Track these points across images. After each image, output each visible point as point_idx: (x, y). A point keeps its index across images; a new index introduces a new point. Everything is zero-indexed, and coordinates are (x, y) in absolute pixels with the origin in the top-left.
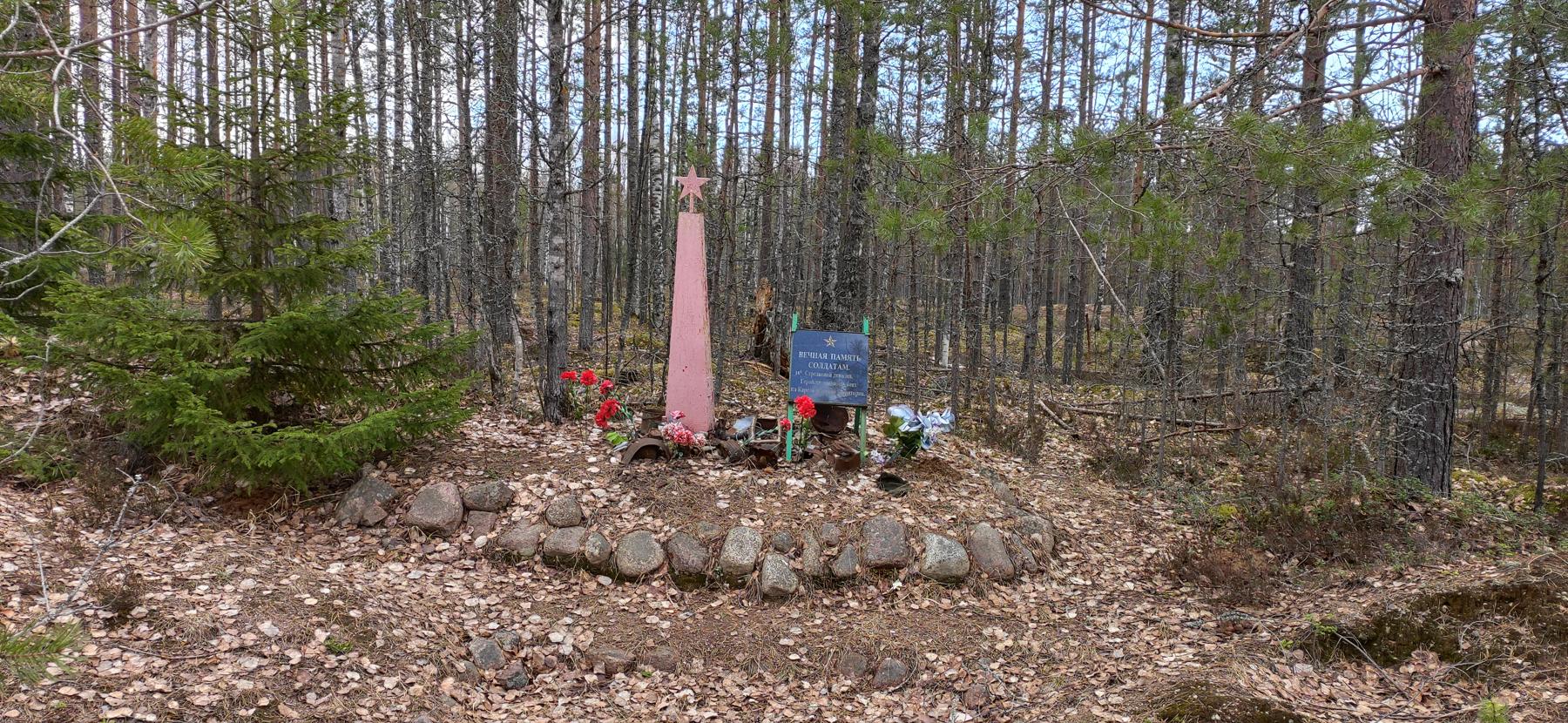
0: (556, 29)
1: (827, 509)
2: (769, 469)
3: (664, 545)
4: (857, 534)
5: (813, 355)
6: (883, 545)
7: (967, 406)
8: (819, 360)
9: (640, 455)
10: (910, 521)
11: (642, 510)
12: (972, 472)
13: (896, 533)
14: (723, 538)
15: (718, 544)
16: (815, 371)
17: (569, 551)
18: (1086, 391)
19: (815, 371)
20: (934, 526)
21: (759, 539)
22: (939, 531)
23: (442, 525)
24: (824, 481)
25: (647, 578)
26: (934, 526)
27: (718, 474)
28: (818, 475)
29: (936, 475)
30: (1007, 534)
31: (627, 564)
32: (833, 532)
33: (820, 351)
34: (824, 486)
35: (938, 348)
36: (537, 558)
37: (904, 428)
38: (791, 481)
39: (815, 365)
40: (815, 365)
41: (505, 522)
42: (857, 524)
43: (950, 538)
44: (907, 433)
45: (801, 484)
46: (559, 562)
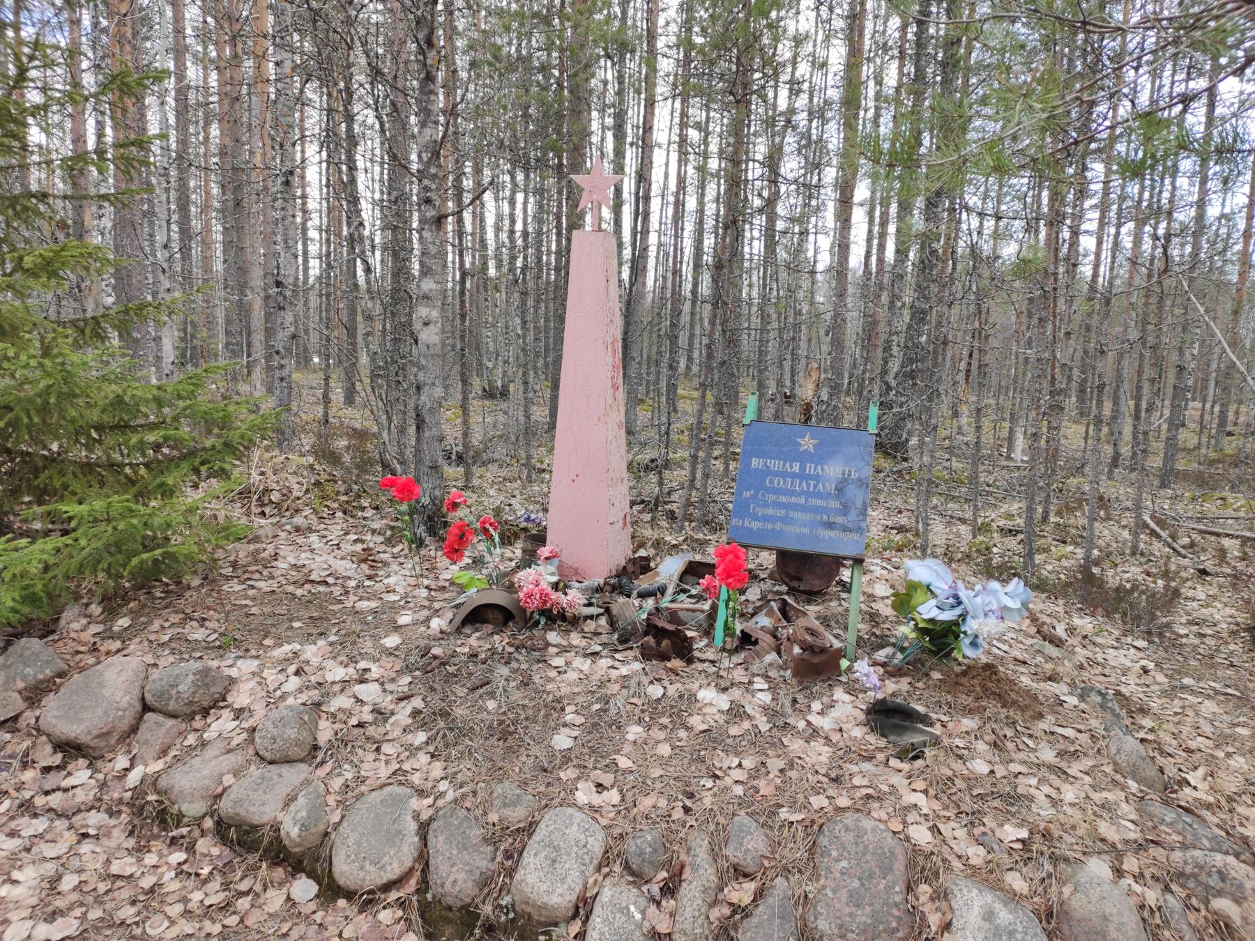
0: (770, 232)
1: (755, 774)
2: (676, 663)
3: (424, 829)
4: (802, 854)
5: (775, 465)
6: (856, 900)
7: (1045, 519)
8: (784, 475)
9: (477, 616)
10: (921, 835)
11: (421, 737)
12: (1061, 689)
13: (886, 870)
14: (530, 828)
15: (511, 843)
16: (778, 492)
17: (256, 820)
18: (1193, 499)
19: (778, 492)
20: (977, 855)
21: (596, 845)
22: (988, 877)
23: (84, 739)
24: (766, 698)
25: (368, 901)
26: (977, 855)
27: (586, 665)
28: (760, 683)
29: (993, 707)
30: (1152, 896)
31: (345, 869)
32: (751, 843)
33: (789, 457)
34: (765, 709)
35: (1011, 439)
36: (209, 823)
37: (928, 610)
38: (707, 695)
39: (778, 482)
40: (778, 482)
41: (191, 739)
42: (808, 826)
43: (1013, 897)
44: (932, 621)
45: (723, 702)
46: (247, 841)
